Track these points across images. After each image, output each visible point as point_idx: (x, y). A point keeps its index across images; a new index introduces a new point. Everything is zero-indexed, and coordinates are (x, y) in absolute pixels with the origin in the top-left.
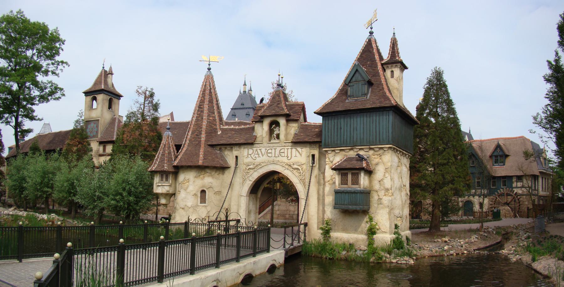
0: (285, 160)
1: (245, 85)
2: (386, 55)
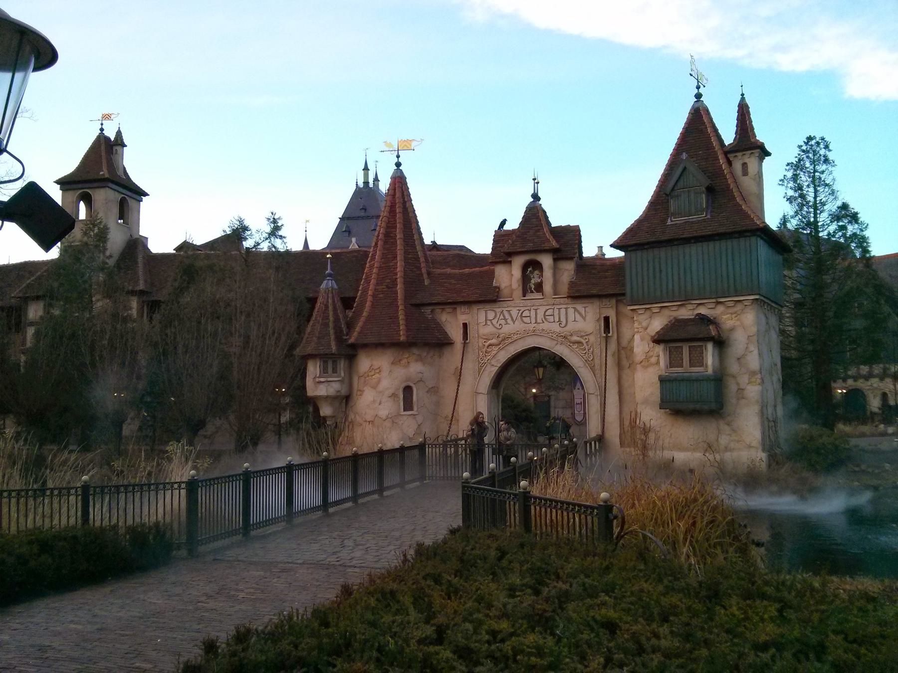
0: (556, 327)
1: (366, 169)
2: (728, 135)
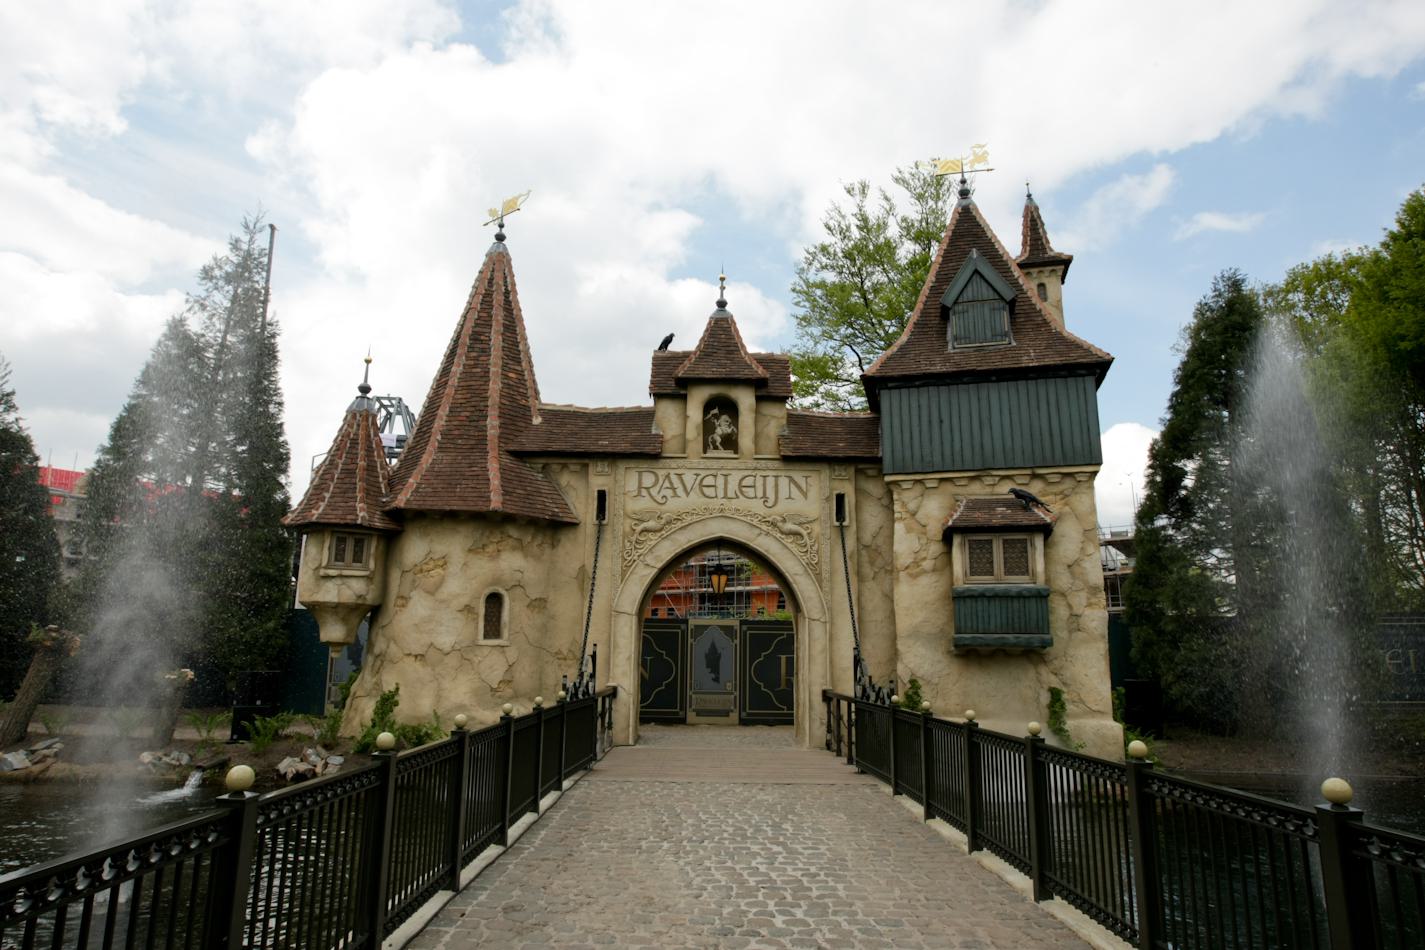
0: (757, 506)
